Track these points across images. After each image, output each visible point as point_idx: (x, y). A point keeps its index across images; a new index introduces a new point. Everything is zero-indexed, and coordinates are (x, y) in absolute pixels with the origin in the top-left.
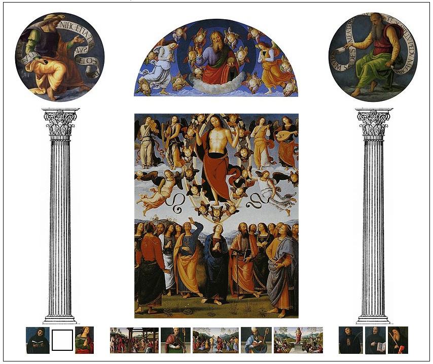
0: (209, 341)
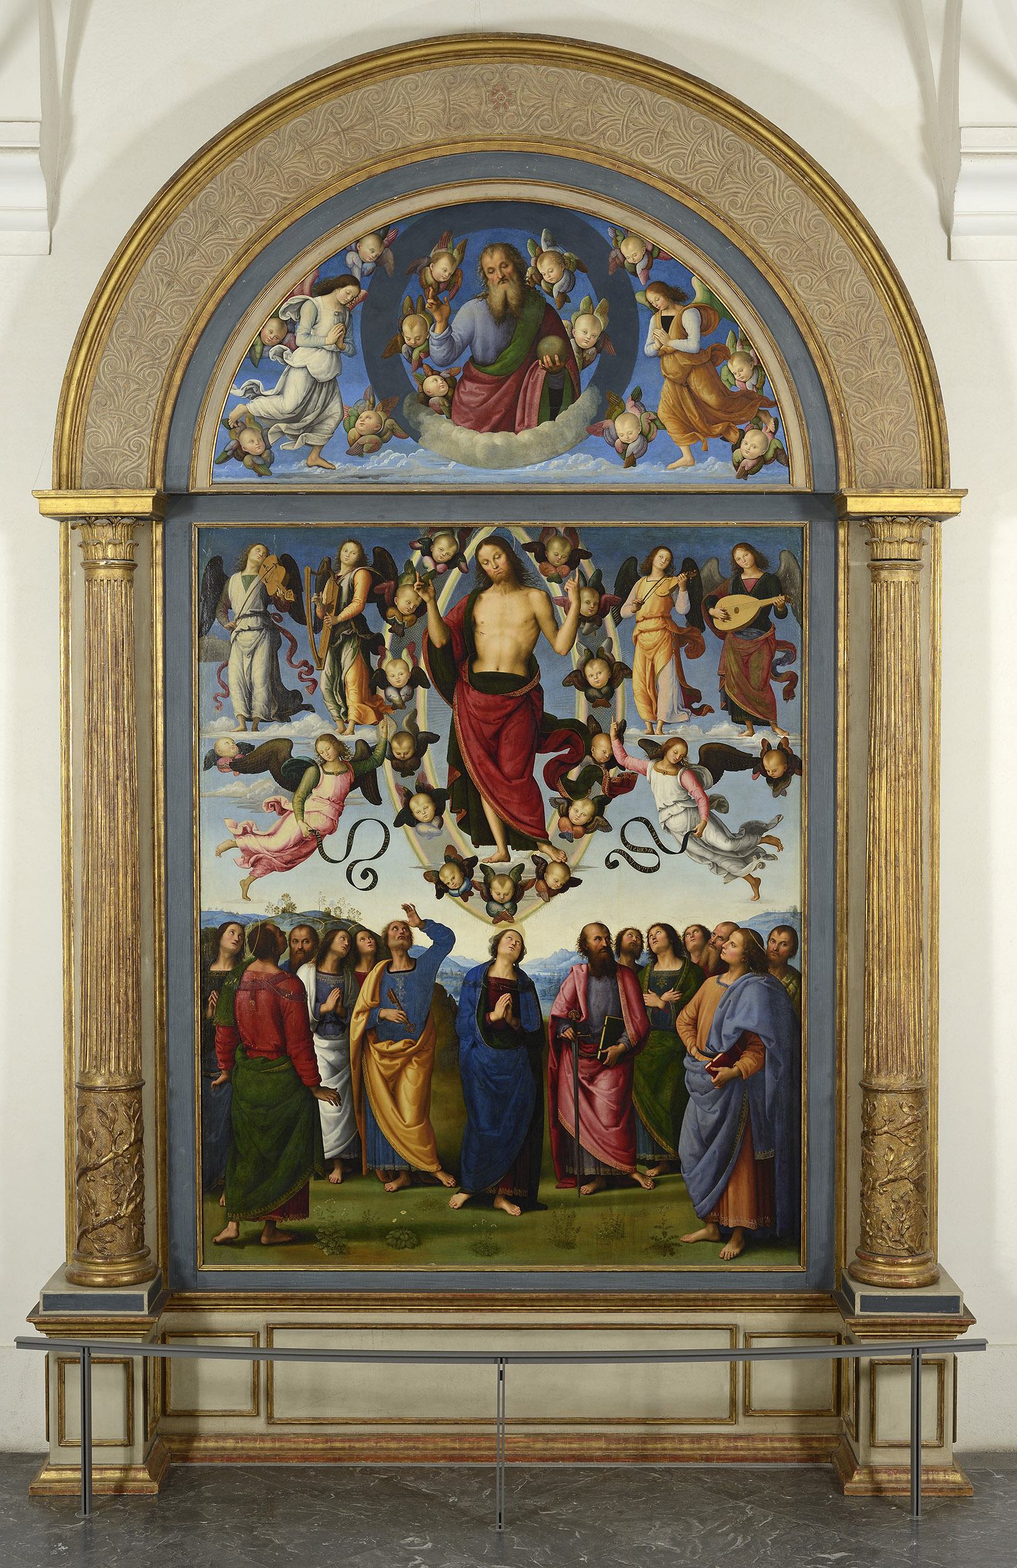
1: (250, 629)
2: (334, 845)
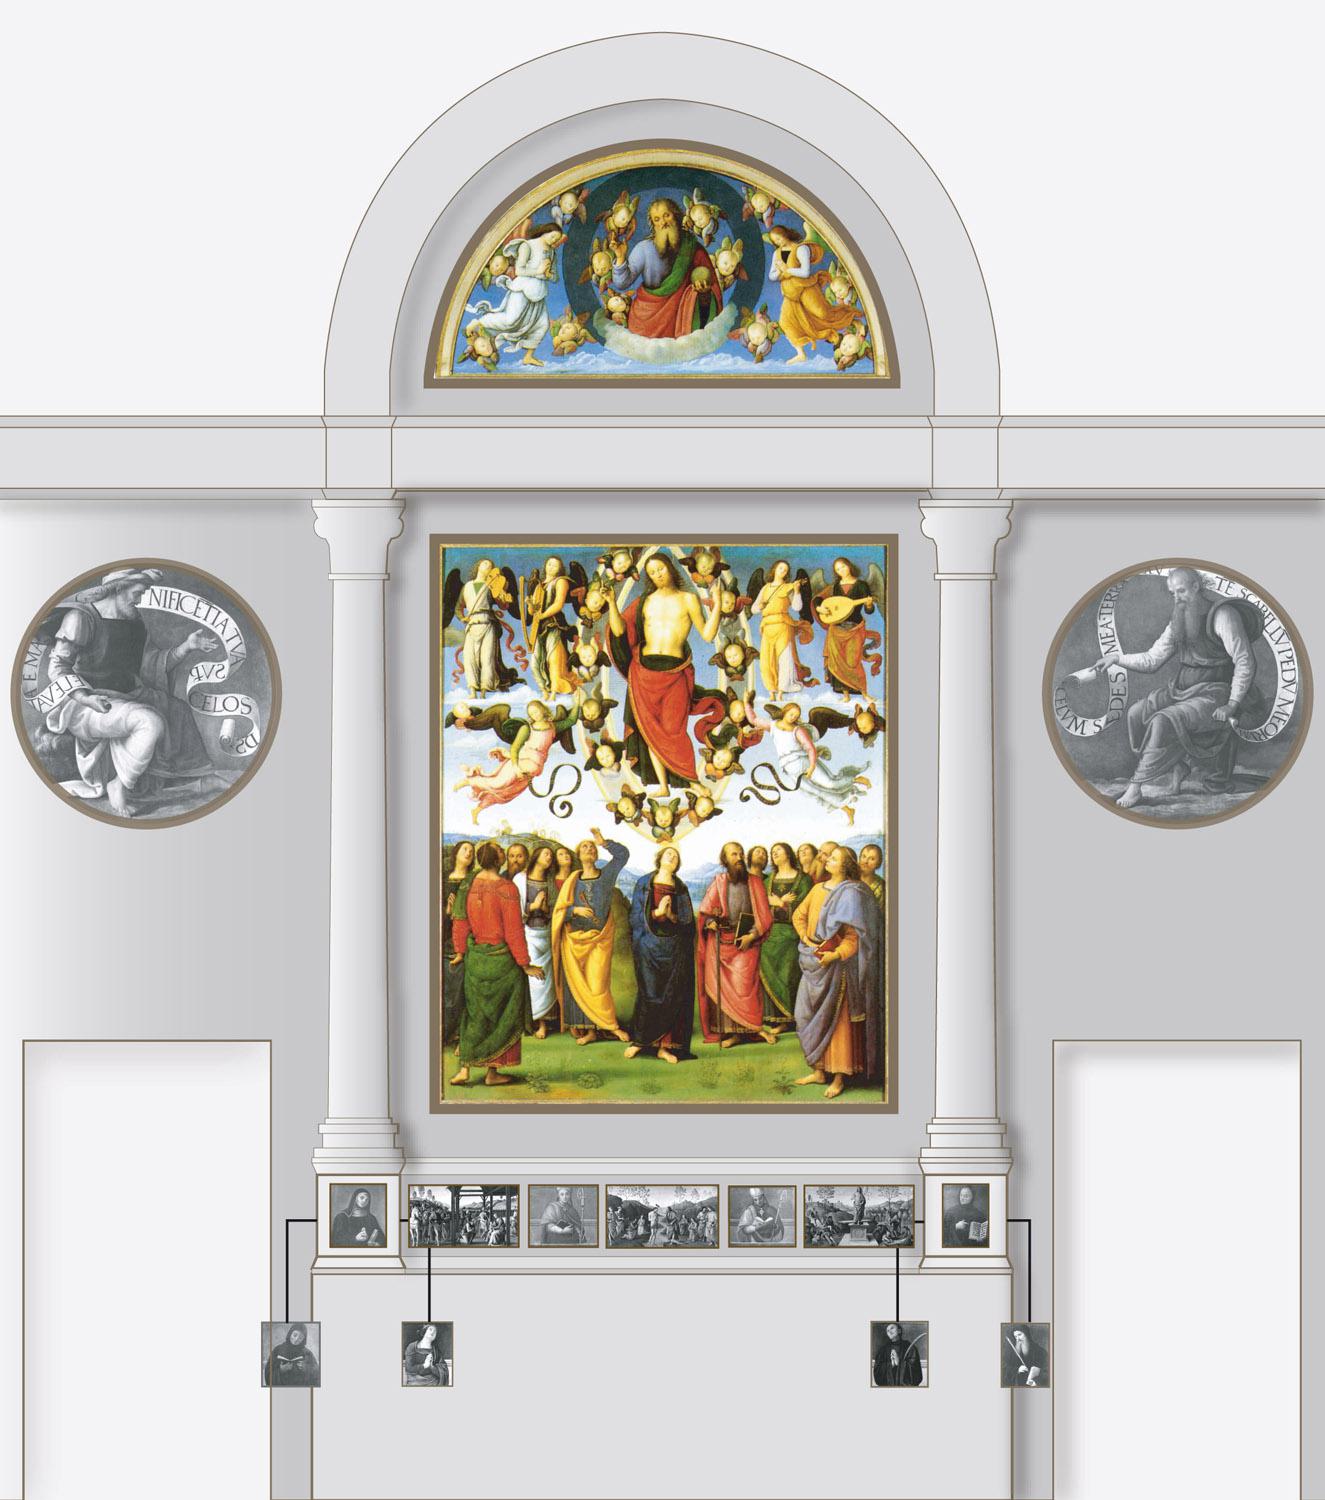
0: (646, 1218)
1: (479, 623)
2: (540, 783)
